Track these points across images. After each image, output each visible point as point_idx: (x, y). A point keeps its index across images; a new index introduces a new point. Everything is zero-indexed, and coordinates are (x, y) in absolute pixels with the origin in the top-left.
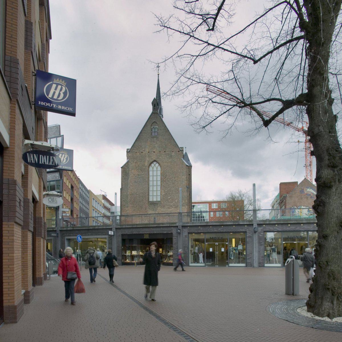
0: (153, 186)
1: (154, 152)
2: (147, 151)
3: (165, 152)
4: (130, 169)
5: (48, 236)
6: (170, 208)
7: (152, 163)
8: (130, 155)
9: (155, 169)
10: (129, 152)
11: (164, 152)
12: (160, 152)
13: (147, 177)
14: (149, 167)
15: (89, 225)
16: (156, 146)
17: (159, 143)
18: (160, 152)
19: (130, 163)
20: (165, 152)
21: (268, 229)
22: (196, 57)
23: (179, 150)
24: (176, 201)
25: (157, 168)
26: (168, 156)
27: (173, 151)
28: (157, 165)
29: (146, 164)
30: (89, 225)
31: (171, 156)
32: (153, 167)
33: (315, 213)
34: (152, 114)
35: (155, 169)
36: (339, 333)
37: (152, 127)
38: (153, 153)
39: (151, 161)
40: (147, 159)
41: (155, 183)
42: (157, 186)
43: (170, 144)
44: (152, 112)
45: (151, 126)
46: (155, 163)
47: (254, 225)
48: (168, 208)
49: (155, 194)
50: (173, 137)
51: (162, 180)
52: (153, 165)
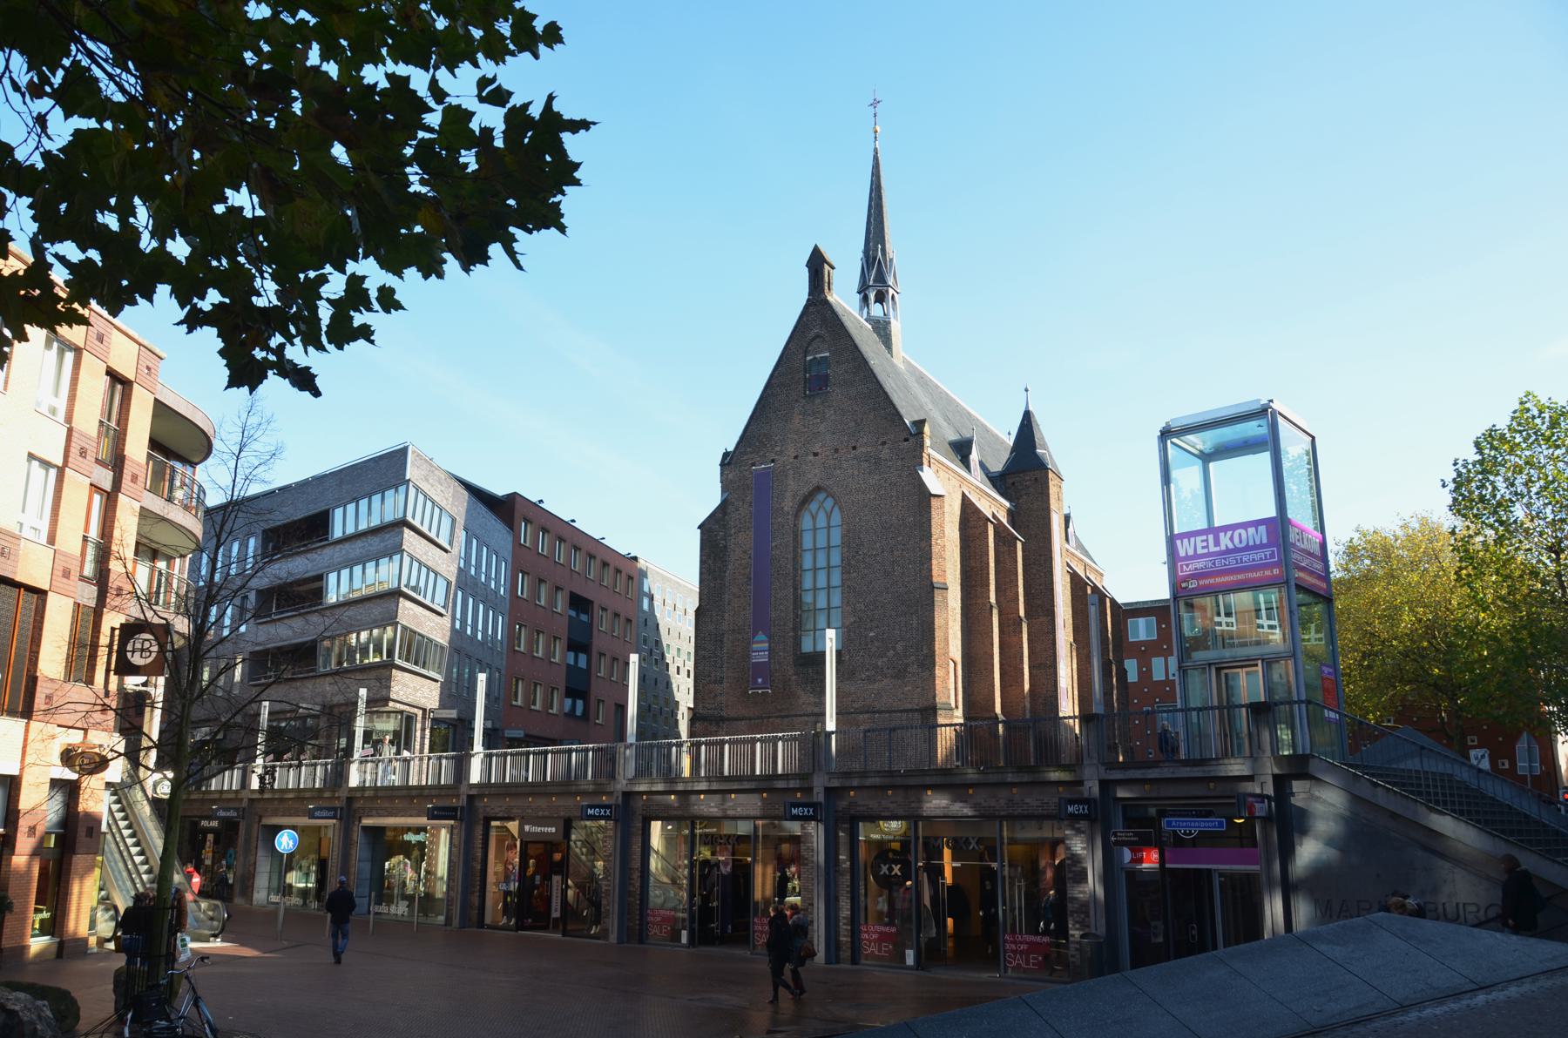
0: (815, 589)
1: (816, 454)
2: (792, 452)
3: (854, 448)
4: (733, 531)
5: (700, 835)
6: (875, 681)
7: (806, 500)
8: (730, 476)
9: (822, 521)
10: (729, 464)
11: (851, 449)
12: (836, 451)
13: (790, 556)
14: (797, 516)
15: (410, 784)
16: (822, 428)
17: (833, 417)
18: (836, 451)
19: (731, 509)
20: (854, 448)
21: (865, 808)
22: (781, 989)
23: (905, 435)
24: (899, 647)
25: (829, 517)
26: (867, 464)
27: (884, 443)
28: (829, 503)
29: (788, 505)
30: (410, 784)
31: (878, 461)
32: (814, 512)
33: (1430, 629)
34: (806, 308)
35: (822, 521)
36: (424, 633)
37: (808, 358)
38: (811, 458)
39: (805, 491)
40: (792, 484)
41: (821, 557)
42: (829, 567)
43: (871, 417)
44: (808, 300)
45: (806, 353)
46: (821, 496)
47: (815, 791)
48: (868, 678)
49: (822, 603)
50: (881, 387)
51: (847, 567)
52: (813, 506)
